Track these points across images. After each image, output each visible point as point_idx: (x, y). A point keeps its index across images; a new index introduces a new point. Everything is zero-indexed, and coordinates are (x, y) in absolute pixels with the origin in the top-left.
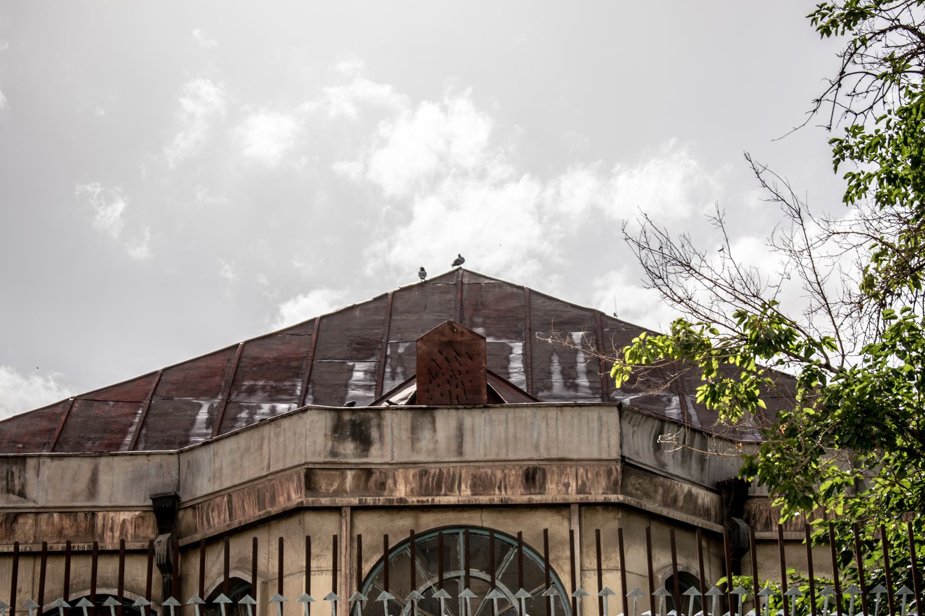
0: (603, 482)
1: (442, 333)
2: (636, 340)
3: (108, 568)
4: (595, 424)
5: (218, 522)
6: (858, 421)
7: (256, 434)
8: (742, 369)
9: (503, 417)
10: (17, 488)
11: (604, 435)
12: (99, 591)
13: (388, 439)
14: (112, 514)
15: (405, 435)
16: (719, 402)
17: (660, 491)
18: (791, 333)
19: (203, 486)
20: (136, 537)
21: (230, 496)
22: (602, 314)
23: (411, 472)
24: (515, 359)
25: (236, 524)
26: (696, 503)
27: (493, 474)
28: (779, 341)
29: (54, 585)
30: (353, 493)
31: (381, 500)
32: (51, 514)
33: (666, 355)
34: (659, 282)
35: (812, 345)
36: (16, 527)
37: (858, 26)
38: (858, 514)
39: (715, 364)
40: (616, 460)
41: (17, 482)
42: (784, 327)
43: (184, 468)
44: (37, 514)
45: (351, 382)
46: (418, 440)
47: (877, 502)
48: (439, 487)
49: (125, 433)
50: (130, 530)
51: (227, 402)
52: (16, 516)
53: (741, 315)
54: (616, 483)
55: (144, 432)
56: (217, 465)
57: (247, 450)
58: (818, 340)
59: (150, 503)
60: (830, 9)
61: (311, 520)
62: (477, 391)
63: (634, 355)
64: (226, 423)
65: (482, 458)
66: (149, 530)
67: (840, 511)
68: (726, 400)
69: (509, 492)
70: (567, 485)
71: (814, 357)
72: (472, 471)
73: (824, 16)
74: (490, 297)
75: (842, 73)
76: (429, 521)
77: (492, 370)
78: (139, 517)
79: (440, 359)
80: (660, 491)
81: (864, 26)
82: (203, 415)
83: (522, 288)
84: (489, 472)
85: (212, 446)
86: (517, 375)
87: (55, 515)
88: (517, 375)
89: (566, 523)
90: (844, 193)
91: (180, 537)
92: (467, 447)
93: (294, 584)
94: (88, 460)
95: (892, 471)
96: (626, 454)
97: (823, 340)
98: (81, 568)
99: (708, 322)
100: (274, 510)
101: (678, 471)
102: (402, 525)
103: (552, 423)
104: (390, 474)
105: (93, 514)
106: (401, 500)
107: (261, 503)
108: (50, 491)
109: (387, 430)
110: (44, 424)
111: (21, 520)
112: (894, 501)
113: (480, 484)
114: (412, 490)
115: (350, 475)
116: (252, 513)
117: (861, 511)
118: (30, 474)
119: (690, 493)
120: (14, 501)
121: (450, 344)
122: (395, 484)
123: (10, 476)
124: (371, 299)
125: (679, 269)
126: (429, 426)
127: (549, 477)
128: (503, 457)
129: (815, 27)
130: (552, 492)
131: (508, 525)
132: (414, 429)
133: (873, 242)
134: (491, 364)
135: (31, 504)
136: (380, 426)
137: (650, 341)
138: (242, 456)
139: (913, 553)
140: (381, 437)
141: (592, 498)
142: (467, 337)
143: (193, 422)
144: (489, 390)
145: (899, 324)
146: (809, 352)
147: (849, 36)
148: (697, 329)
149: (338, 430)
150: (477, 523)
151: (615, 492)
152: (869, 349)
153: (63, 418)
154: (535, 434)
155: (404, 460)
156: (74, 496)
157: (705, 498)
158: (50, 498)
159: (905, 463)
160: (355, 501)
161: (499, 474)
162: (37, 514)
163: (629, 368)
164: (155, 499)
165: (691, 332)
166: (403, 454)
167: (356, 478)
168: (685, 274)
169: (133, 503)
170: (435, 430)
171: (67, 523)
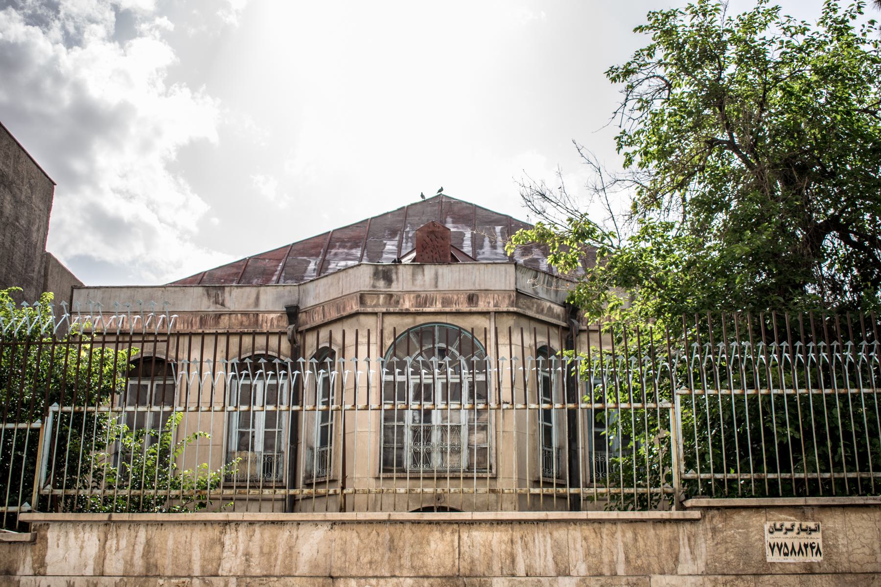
0: (507, 301)
1: (429, 227)
2: (517, 232)
3: (261, 341)
4: (503, 273)
5: (318, 319)
6: (625, 274)
7: (336, 276)
8: (570, 247)
9: (458, 269)
10: (221, 302)
11: (508, 278)
12: (256, 353)
13: (400, 279)
14: (266, 315)
15: (409, 277)
16: (558, 263)
17: (535, 306)
18: (594, 229)
19: (310, 302)
20: (278, 326)
21: (323, 306)
22: (511, 218)
23: (412, 296)
24: (467, 240)
25: (326, 320)
26: (553, 312)
27: (452, 297)
28: (588, 233)
29: (234, 349)
30: (383, 306)
31: (397, 310)
32: (237, 314)
33: (533, 240)
34: (529, 203)
35: (605, 235)
36: (220, 321)
37: (630, 78)
38: (626, 319)
39: (557, 245)
40: (513, 291)
41: (220, 298)
42: (591, 226)
43: (301, 293)
44: (230, 314)
45: (385, 250)
46: (416, 280)
47: (636, 313)
48: (426, 303)
49: (272, 275)
50: (275, 323)
51: (324, 260)
52: (220, 315)
53: (571, 220)
54: (513, 302)
55: (283, 274)
56: (317, 291)
57: (332, 284)
58: (607, 233)
59: (285, 309)
60: (617, 69)
61: (362, 318)
62: (446, 256)
63: (517, 240)
64: (323, 270)
65: (447, 289)
66: (284, 323)
67: (617, 318)
68: (562, 262)
69: (460, 306)
70: (489, 303)
71: (605, 241)
72: (442, 295)
73: (613, 72)
74: (456, 209)
75: (627, 99)
76: (421, 320)
77: (455, 246)
78: (279, 316)
79: (428, 240)
80: (535, 306)
81: (633, 78)
82: (312, 266)
83: (471, 204)
84: (450, 296)
85: (315, 282)
86: (467, 248)
87: (239, 315)
88: (467, 248)
89: (488, 321)
90: (623, 163)
91: (300, 326)
92: (440, 284)
93: (350, 352)
94: (255, 288)
95: (643, 298)
96: (518, 288)
97: (610, 233)
98: (247, 340)
99: (553, 224)
100: (345, 314)
101: (544, 296)
102: (408, 322)
103: (482, 272)
104: (402, 297)
105: (257, 314)
106: (407, 309)
107: (338, 311)
108: (236, 303)
109: (400, 275)
110: (234, 270)
111: (222, 317)
112: (643, 313)
113: (446, 302)
114: (412, 305)
115: (382, 297)
116: (334, 315)
117: (628, 317)
118: (227, 295)
119: (550, 307)
120: (219, 308)
121: (433, 232)
122: (404, 301)
123: (217, 296)
124: (396, 209)
125: (540, 197)
126: (421, 273)
127: (480, 299)
128: (457, 288)
129: (608, 78)
130: (482, 306)
131: (465, 323)
132: (413, 275)
133: (637, 185)
134: (453, 242)
135: (227, 310)
136: (397, 273)
137: (525, 233)
138: (329, 287)
139: (652, 339)
140: (397, 278)
141: (501, 309)
142: (441, 229)
143: (306, 269)
144: (452, 255)
145: (647, 226)
146: (603, 239)
147: (626, 83)
148: (547, 227)
149: (376, 275)
150: (444, 321)
151: (512, 306)
152: (632, 238)
153: (243, 267)
154: (474, 277)
155: (409, 290)
156: (248, 306)
157: (558, 309)
158: (236, 306)
159: (649, 294)
160: (384, 310)
161: (455, 297)
162: (230, 314)
163: (514, 246)
164: (287, 308)
165: (544, 229)
166: (408, 287)
167: (385, 298)
168: (543, 200)
169: (277, 309)
170: (424, 275)
171: (245, 319)
